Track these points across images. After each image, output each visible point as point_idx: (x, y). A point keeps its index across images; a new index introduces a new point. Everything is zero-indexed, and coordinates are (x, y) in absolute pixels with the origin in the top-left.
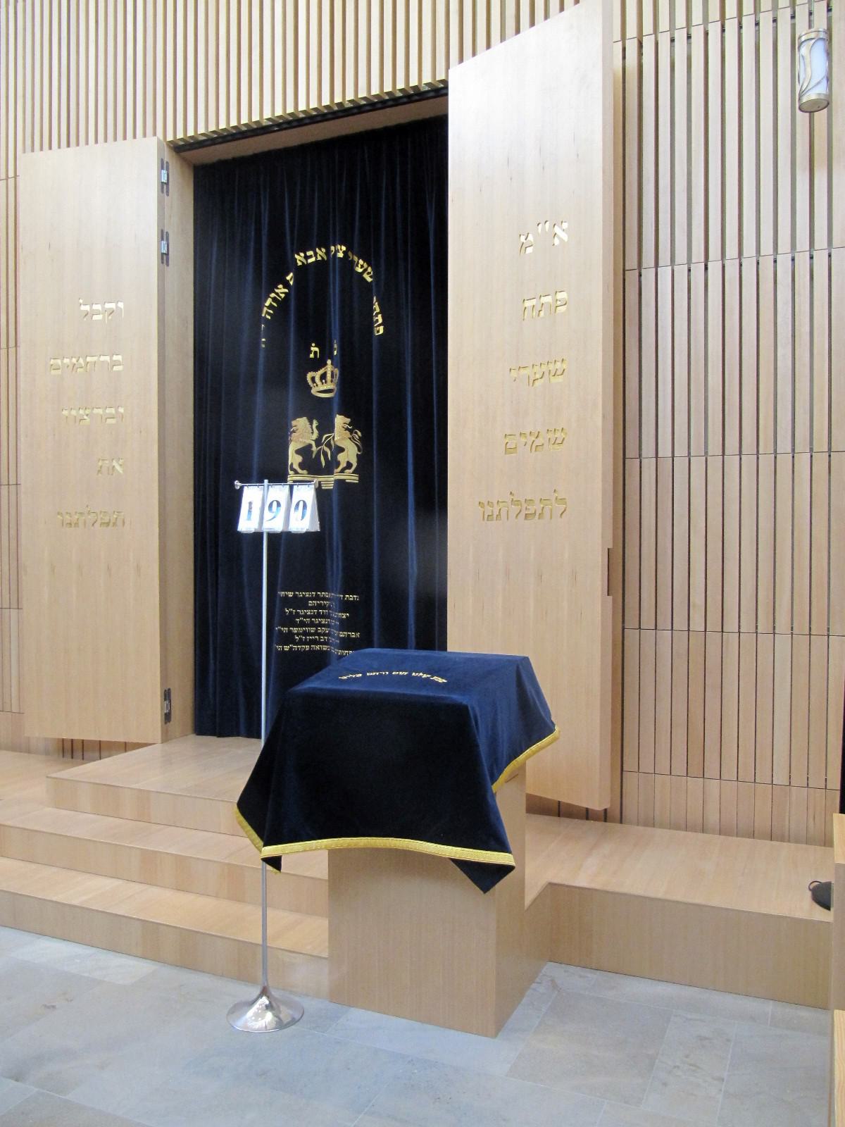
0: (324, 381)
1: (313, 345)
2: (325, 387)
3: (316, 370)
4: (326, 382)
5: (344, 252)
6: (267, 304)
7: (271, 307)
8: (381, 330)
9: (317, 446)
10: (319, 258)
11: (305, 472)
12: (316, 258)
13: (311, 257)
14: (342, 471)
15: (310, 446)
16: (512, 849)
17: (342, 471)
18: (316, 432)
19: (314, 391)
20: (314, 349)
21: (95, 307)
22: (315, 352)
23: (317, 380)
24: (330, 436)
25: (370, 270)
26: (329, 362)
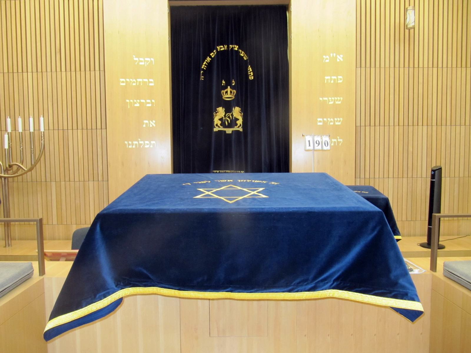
0: (227, 94)
1: (223, 80)
2: (227, 96)
3: (224, 90)
4: (227, 94)
5: (238, 48)
6: (204, 64)
7: (205, 65)
8: (253, 78)
9: (225, 117)
10: (225, 49)
11: (222, 127)
12: (224, 49)
13: (222, 48)
14: (239, 127)
15: (223, 117)
16: (420, 300)
17: (239, 127)
18: (224, 112)
19: (223, 98)
20: (224, 82)
21: (141, 59)
22: (224, 83)
23: (224, 93)
24: (229, 114)
25: (245, 55)
26: (229, 87)
